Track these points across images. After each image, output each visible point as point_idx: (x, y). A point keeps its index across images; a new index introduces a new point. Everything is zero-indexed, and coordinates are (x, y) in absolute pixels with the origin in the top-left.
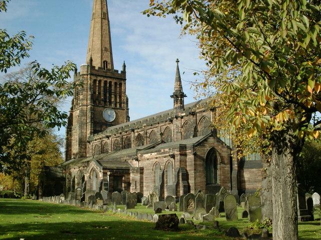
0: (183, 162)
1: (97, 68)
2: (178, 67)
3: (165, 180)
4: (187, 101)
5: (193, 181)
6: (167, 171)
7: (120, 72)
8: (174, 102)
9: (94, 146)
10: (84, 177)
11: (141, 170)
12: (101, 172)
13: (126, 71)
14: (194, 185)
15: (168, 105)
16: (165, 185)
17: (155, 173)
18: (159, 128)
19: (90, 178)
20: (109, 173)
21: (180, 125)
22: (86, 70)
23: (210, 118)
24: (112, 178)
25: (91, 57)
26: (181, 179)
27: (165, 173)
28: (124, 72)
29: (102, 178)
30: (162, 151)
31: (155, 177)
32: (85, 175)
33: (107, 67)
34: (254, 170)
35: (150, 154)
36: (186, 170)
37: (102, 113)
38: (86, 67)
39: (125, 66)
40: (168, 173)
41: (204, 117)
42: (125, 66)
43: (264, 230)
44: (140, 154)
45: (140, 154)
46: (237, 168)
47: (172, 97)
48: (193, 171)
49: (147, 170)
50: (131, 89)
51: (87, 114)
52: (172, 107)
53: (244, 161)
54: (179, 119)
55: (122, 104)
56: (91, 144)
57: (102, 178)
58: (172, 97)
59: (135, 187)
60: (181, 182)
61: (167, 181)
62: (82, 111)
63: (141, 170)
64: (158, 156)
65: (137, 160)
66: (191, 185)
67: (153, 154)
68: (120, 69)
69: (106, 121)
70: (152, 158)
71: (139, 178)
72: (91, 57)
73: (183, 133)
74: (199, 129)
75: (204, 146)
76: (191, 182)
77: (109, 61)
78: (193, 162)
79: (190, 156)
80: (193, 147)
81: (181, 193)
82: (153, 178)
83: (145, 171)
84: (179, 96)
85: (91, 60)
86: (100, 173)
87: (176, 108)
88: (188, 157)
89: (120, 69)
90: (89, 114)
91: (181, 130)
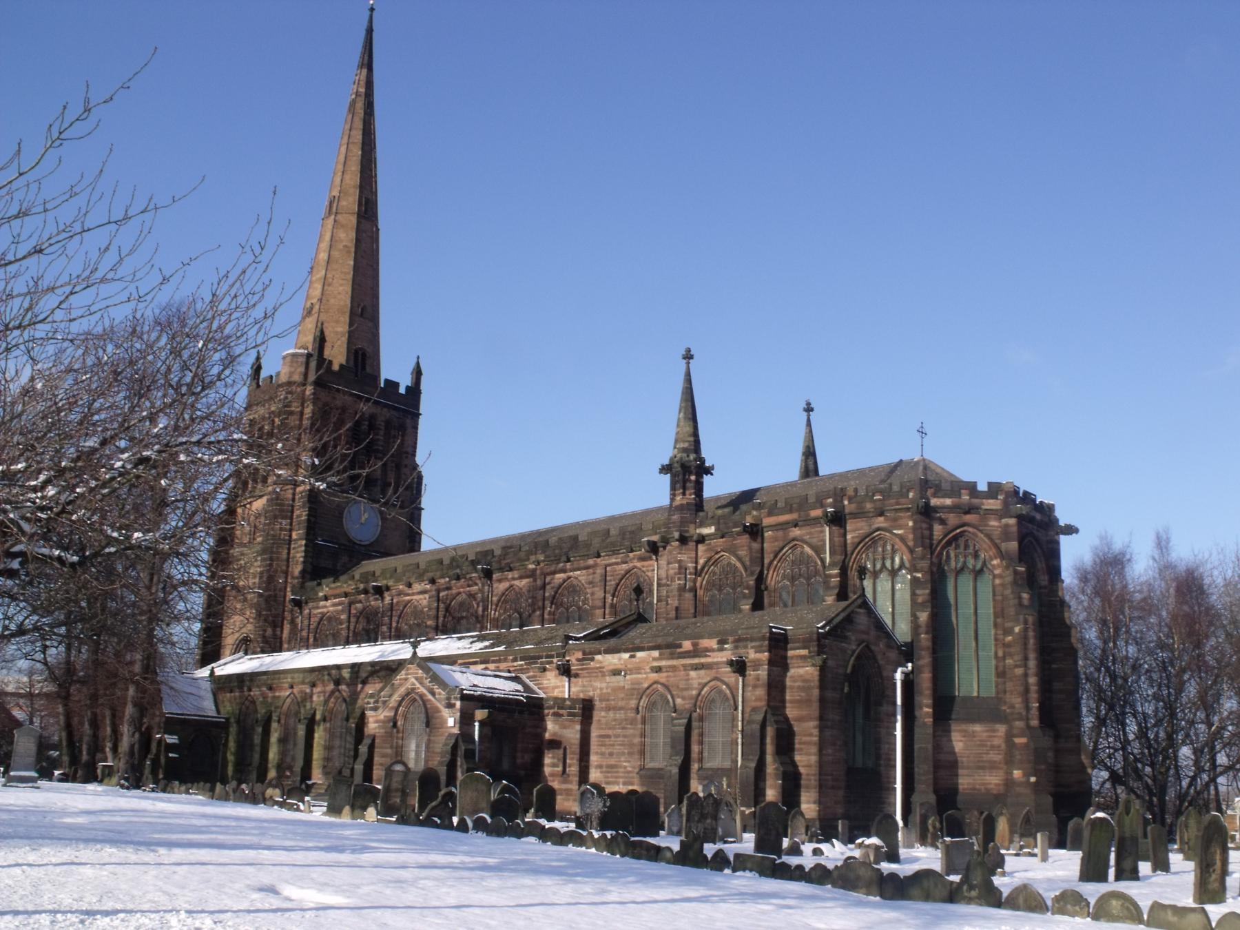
0: (776, 687)
1: (336, 367)
2: (370, 31)
3: (695, 748)
4: (713, 488)
5: (814, 759)
6: (701, 719)
7: (402, 390)
8: (673, 488)
9: (314, 620)
10: (362, 720)
11: (586, 709)
12: (450, 706)
13: (422, 388)
14: (814, 770)
15: (656, 493)
16: (695, 766)
17: (644, 722)
18: (599, 571)
19: (395, 725)
20: (481, 714)
21: (691, 565)
22: (302, 369)
23: (819, 550)
24: (487, 730)
25: (418, 364)
26: (770, 748)
27: (695, 724)
28: (414, 391)
29: (456, 731)
30: (687, 645)
31: (643, 735)
32: (368, 713)
33: (364, 368)
34: (977, 728)
35: (626, 656)
36: (787, 719)
37: (341, 514)
38: (303, 359)
39: (418, 373)
40: (706, 724)
41: (794, 543)
42: (418, 373)
43: (777, 600)
44: (580, 655)
45: (580, 655)
46: (929, 720)
47: (665, 469)
48: (816, 723)
49: (608, 709)
50: (436, 448)
51: (292, 512)
52: (665, 501)
53: (952, 699)
54: (692, 544)
55: (400, 487)
56: (307, 611)
57: (456, 731)
58: (665, 469)
59: (560, 769)
60: (769, 758)
61: (701, 753)
62: (276, 500)
63: (586, 709)
64: (663, 663)
65: (565, 671)
66: (802, 770)
67: (640, 654)
68: (405, 381)
69: (350, 541)
70: (638, 670)
71: (578, 736)
72: (418, 364)
73: (700, 593)
74: (772, 579)
75: (846, 638)
76: (806, 759)
77: (369, 350)
78: (816, 692)
79: (801, 671)
80: (819, 640)
81: (771, 794)
82: (637, 740)
83: (598, 715)
84: (688, 470)
85: (810, 453)
86: (445, 712)
87: (681, 508)
88: (792, 672)
89: (405, 381)
90: (301, 514)
91: (695, 581)
